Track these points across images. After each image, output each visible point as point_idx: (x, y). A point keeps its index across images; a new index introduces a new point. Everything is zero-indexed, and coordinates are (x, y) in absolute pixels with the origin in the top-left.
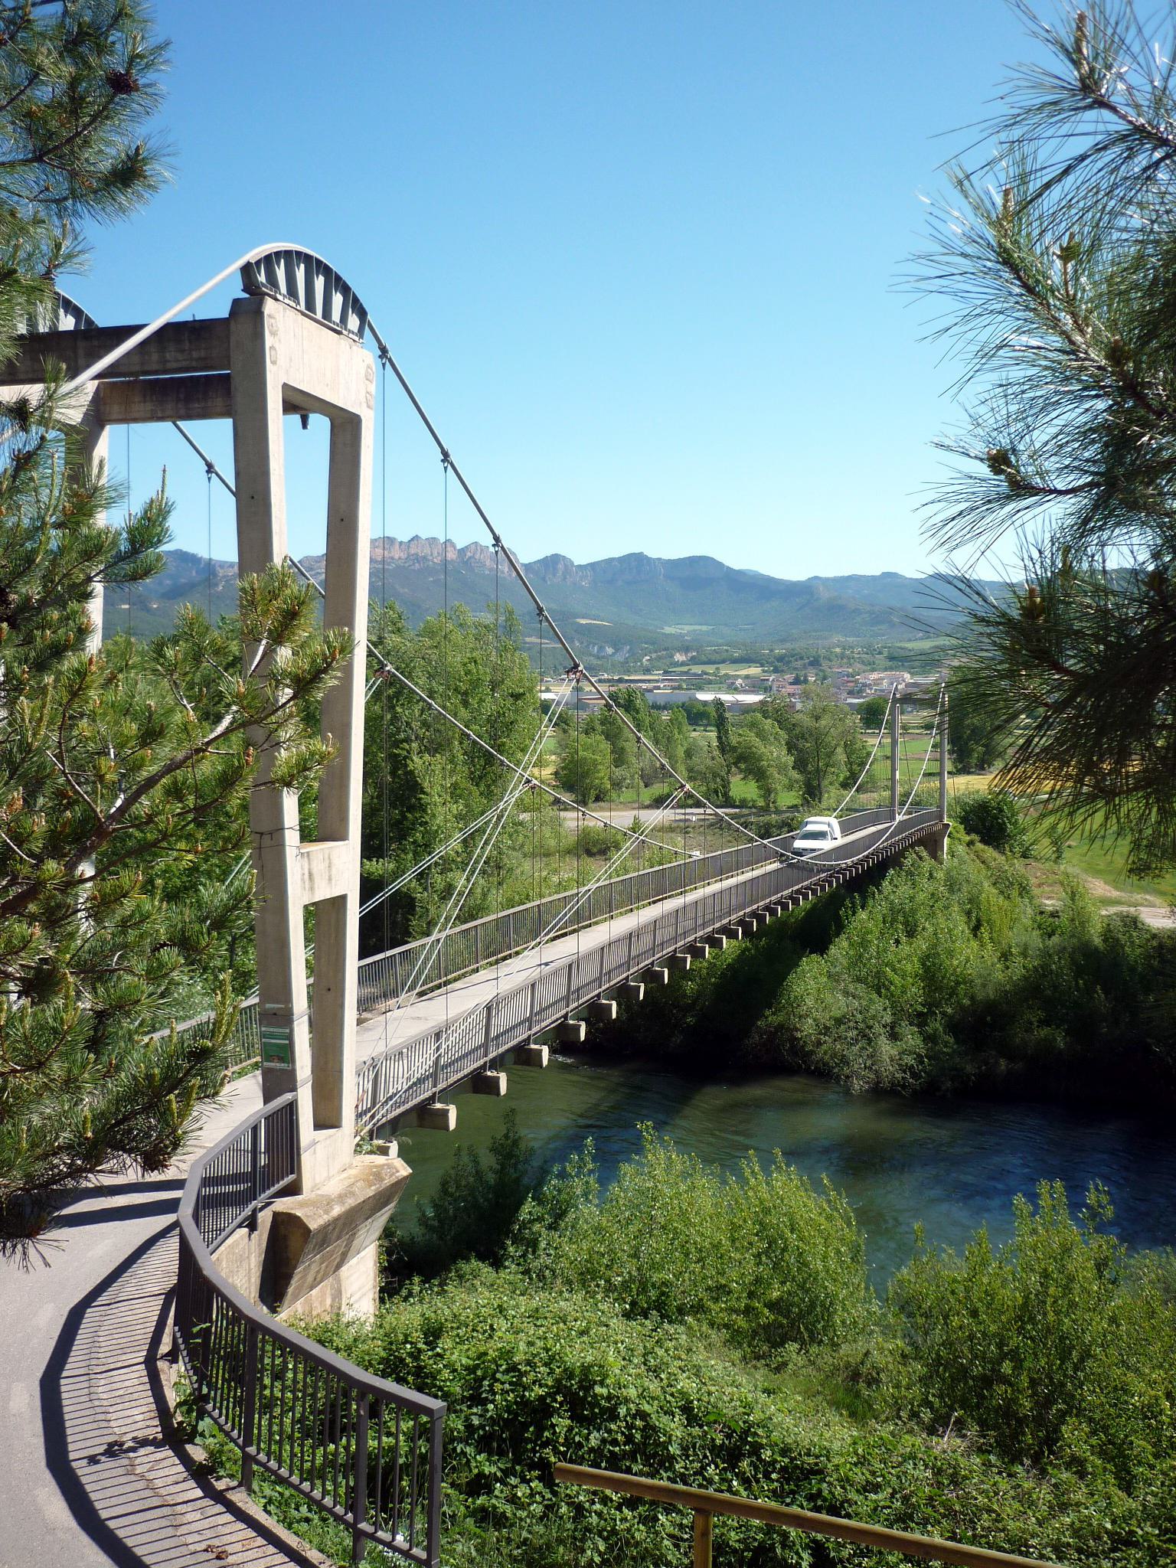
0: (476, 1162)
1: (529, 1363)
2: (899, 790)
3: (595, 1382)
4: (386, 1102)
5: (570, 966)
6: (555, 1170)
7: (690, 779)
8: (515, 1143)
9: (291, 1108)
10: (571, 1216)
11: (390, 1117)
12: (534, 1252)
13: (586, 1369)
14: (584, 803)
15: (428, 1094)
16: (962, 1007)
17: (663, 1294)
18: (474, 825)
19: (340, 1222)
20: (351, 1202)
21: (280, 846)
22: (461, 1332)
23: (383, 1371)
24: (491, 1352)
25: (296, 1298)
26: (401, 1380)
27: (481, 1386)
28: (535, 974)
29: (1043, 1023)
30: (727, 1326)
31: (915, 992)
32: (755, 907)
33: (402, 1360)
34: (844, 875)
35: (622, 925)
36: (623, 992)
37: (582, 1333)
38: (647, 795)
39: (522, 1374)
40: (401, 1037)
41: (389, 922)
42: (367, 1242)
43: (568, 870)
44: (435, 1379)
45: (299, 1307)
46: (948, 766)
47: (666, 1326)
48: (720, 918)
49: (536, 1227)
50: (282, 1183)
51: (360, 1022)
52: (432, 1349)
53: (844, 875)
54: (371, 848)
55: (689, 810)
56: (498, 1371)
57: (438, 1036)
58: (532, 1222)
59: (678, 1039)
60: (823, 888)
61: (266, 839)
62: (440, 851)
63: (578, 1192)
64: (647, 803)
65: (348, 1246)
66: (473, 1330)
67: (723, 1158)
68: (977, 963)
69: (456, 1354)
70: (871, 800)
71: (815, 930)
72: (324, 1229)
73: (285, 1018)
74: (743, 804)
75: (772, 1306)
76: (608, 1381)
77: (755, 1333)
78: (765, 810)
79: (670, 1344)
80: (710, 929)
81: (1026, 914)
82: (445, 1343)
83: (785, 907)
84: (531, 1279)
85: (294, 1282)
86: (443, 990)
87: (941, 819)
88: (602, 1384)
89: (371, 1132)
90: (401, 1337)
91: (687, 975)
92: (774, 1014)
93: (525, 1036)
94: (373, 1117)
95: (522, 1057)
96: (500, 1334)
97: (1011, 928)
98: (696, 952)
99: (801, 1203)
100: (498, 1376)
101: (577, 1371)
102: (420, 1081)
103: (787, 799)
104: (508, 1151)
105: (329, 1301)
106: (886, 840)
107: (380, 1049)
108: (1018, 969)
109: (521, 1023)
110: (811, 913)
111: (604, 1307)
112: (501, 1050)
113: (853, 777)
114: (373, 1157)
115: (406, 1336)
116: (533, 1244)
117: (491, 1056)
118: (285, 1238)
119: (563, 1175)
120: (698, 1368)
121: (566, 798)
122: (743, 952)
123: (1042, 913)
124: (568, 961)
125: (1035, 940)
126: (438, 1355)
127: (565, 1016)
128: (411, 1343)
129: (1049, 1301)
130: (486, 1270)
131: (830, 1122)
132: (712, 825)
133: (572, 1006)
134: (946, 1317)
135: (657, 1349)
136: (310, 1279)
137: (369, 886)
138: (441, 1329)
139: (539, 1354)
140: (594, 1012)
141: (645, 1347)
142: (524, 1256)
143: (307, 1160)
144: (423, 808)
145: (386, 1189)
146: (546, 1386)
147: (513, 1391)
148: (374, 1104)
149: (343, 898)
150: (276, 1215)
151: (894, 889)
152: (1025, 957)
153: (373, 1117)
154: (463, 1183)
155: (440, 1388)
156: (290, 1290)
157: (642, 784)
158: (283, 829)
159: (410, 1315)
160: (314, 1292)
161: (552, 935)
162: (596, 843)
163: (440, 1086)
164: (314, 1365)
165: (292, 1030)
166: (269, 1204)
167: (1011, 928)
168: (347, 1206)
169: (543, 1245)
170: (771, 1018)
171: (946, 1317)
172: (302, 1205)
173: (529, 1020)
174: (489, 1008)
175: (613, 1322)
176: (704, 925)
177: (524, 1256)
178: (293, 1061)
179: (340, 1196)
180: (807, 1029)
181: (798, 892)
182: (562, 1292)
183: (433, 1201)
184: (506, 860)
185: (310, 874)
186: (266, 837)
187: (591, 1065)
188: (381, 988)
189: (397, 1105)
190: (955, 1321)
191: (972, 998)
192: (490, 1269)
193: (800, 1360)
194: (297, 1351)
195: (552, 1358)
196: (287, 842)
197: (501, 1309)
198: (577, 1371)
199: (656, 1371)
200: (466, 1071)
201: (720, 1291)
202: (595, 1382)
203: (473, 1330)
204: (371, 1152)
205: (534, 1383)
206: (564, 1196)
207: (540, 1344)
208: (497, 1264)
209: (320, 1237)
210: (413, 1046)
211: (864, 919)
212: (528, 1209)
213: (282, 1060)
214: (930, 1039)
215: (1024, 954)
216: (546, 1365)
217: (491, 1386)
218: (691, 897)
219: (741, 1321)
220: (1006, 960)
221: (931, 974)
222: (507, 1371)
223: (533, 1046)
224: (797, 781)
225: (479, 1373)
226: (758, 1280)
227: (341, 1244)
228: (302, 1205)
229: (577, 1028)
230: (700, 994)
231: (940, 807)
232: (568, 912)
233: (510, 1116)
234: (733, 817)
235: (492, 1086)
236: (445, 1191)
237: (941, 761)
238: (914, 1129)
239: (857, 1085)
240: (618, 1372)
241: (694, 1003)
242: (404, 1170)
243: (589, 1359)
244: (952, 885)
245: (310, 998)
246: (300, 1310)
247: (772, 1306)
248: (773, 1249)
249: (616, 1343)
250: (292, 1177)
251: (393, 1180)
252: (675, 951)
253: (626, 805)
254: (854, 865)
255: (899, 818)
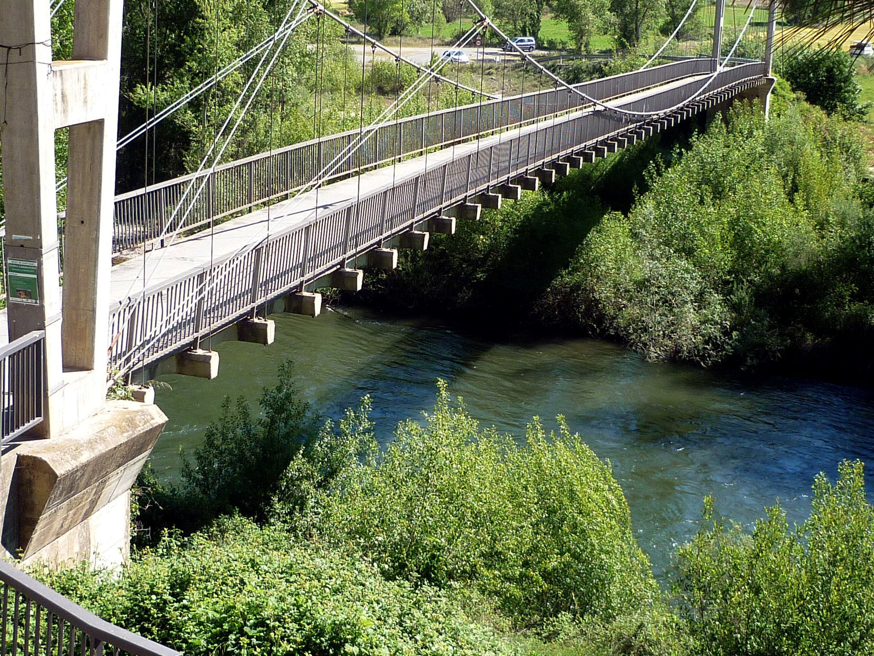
0: (246, 414)
1: (278, 619)
2: (723, 39)
3: (346, 641)
4: (143, 345)
5: (349, 209)
6: (328, 424)
7: (496, 15)
8: (288, 397)
9: (39, 347)
10: (342, 475)
11: (147, 361)
12: (301, 509)
13: (337, 628)
14: (379, 36)
15: (190, 339)
16: (770, 276)
17: (433, 557)
18: (253, 52)
19: (90, 469)
20: (102, 449)
21: (31, 62)
22: (210, 586)
23: (126, 621)
24: (238, 605)
25: (41, 544)
26: (144, 631)
27: (227, 640)
28: (309, 217)
29: (855, 297)
30: (497, 593)
31: (724, 258)
32: (555, 156)
33: (147, 611)
34: (655, 127)
35: (410, 168)
36: (406, 241)
37: (336, 591)
38: (448, 30)
39: (270, 629)
40: (160, 277)
41: (153, 154)
42: (119, 490)
43: (353, 108)
44: (180, 630)
45: (45, 554)
46: (777, 15)
47: (425, 588)
48: (516, 167)
49: (305, 485)
50: (28, 426)
51: (115, 262)
52: (179, 601)
53: (655, 127)
54: (134, 70)
55: (487, 50)
56: (245, 625)
57: (201, 277)
58: (300, 479)
59: (466, 294)
60: (630, 140)
61: (14, 55)
62: (217, 77)
63: (352, 450)
64: (448, 39)
65: (98, 494)
66: (223, 583)
67: (505, 419)
68: (793, 232)
69: (203, 606)
70: (689, 48)
71: (619, 189)
72: (72, 475)
73: (35, 251)
74: (552, 46)
75: (546, 576)
76: (359, 640)
77: (528, 602)
78: (576, 53)
79: (428, 606)
80: (505, 178)
81: (848, 182)
82: (192, 595)
83: (588, 158)
84: (296, 537)
85: (39, 528)
86: (209, 231)
87: (766, 72)
88: (353, 642)
89: (126, 376)
90: (147, 588)
91: (480, 227)
92: (569, 273)
93: (297, 282)
94: (128, 360)
95: (293, 303)
96: (249, 588)
97: (830, 195)
98: (488, 201)
99: (588, 475)
100: (246, 629)
101: (328, 629)
102: (181, 325)
103: (600, 42)
104: (280, 406)
105: (77, 549)
106: (704, 92)
107: (136, 290)
108: (834, 239)
109: (295, 268)
110: (617, 167)
111: (362, 566)
112: (271, 296)
113: (675, 20)
114: (127, 403)
115: (152, 587)
116: (301, 502)
117: (259, 302)
118: (30, 482)
119: (338, 433)
120: (456, 631)
121: (359, 29)
122: (540, 207)
123: (865, 180)
124: (347, 205)
125: (856, 209)
126: (185, 607)
127: (342, 263)
128: (157, 594)
129: (835, 579)
130: (250, 527)
131: (621, 390)
132: (517, 67)
133: (349, 254)
134: (725, 592)
135: (414, 611)
136: (56, 525)
137: (130, 114)
138: (189, 582)
139: (289, 609)
140: (374, 261)
141: (402, 608)
142: (291, 513)
143: (55, 403)
144: (199, 32)
145: (139, 437)
146: (295, 642)
147: (259, 646)
148: (129, 347)
149: (100, 123)
150: (20, 459)
151: (708, 148)
152: (843, 227)
153: (128, 360)
154: (231, 435)
155: (185, 641)
156: (35, 536)
157: (444, 19)
158: (34, 43)
159: (157, 568)
160: (61, 539)
161: (327, 178)
162: (388, 79)
163: (203, 331)
164: (57, 615)
165: (40, 264)
166: (13, 447)
167: (830, 195)
168: (96, 453)
169: (311, 503)
170: (566, 279)
171: (725, 592)
172: (48, 449)
173: (302, 266)
174: (258, 250)
175: (370, 582)
176: (498, 174)
177: (291, 513)
178: (41, 297)
179: (90, 442)
180: (604, 292)
181: (603, 143)
182: (318, 549)
183: (197, 453)
184: (290, 95)
185: (63, 96)
186: (14, 53)
187: (366, 318)
188: (143, 221)
189: (154, 349)
190: (736, 597)
191: (783, 268)
192: (254, 525)
193: (573, 631)
194: (42, 602)
195: (302, 615)
196: (38, 58)
197: (254, 564)
198: (328, 629)
199: (411, 633)
200: (231, 317)
201: (493, 557)
202: (346, 641)
203: (223, 583)
204: (126, 398)
205: (282, 638)
206: (336, 455)
207: (291, 600)
208: (262, 520)
209: (68, 483)
210: (175, 288)
211: (676, 179)
212: (297, 464)
213: (29, 295)
214: (735, 308)
215: (842, 224)
216: (295, 621)
217: (237, 640)
218: (486, 143)
219: (513, 589)
220: (822, 228)
221: (740, 238)
222: (255, 626)
223: (305, 294)
224: (614, 24)
225: (226, 626)
226: (535, 549)
227: (91, 490)
228: (48, 449)
229: (354, 277)
230: (493, 248)
231: (766, 59)
232: (347, 152)
233: (286, 371)
234: (540, 59)
235: (259, 334)
236: (210, 443)
237: (771, 13)
238: (717, 402)
239: (654, 353)
240: (371, 631)
241: (487, 256)
242: (160, 418)
243: (342, 617)
244: (771, 145)
245: (61, 231)
246: (45, 557)
247: (546, 576)
248: (553, 520)
249: (371, 602)
250: (38, 420)
251: (148, 427)
252: (465, 199)
253: (423, 41)
254: (667, 117)
255: (720, 69)
